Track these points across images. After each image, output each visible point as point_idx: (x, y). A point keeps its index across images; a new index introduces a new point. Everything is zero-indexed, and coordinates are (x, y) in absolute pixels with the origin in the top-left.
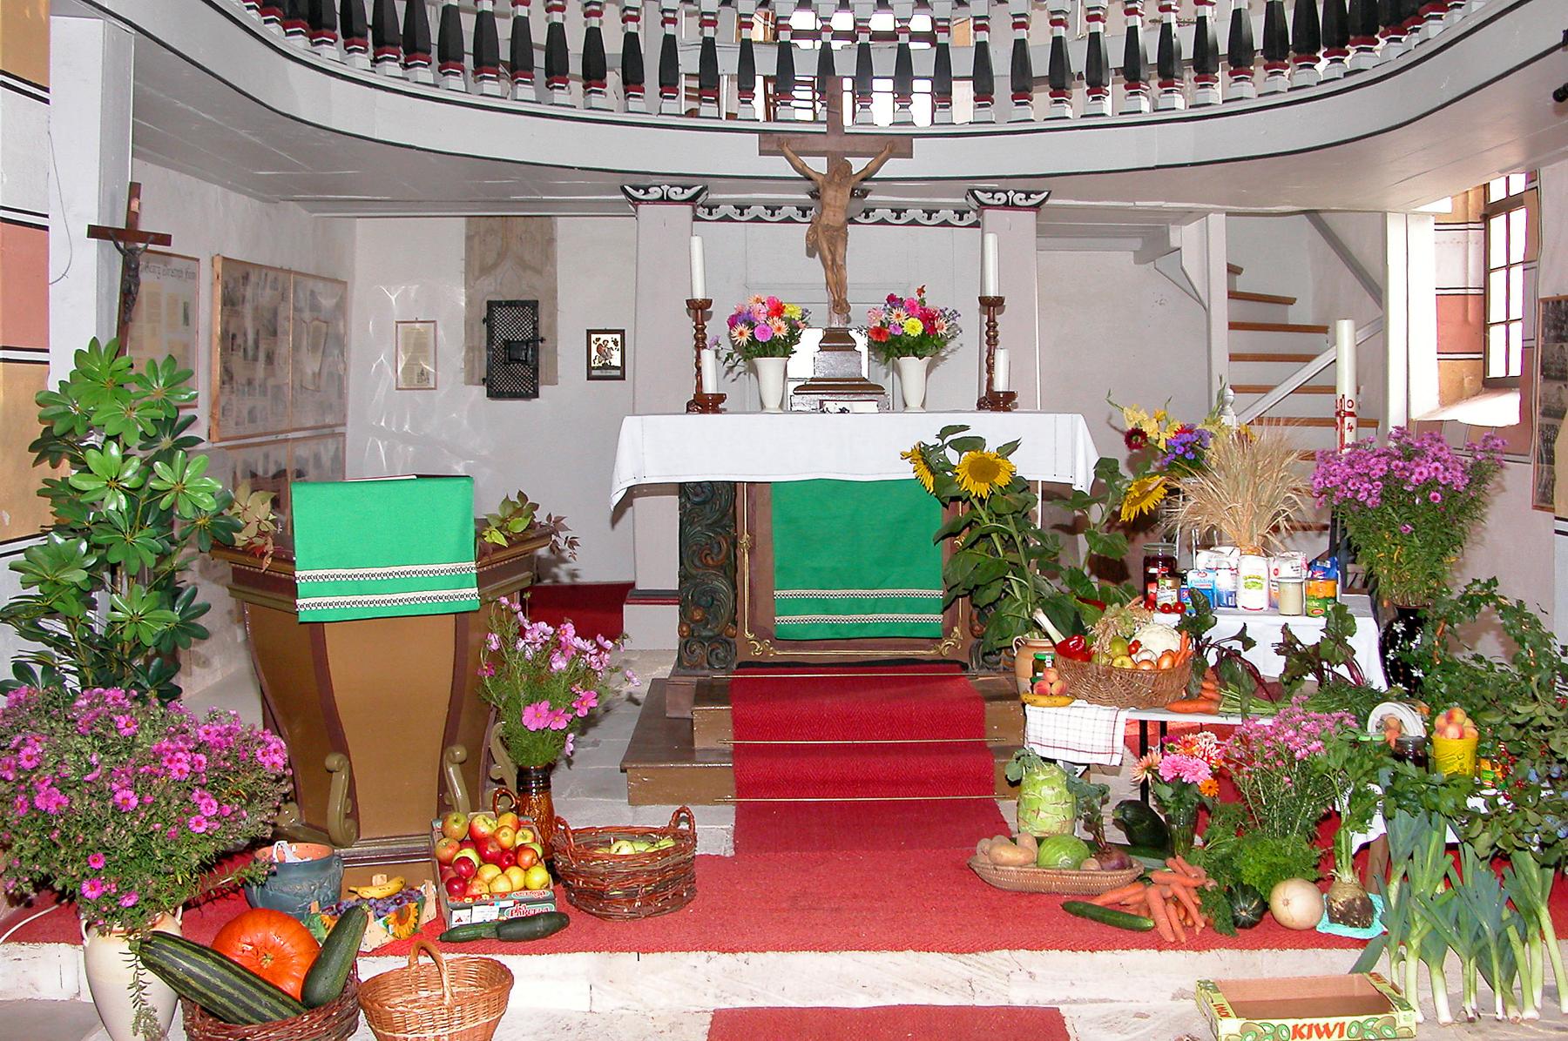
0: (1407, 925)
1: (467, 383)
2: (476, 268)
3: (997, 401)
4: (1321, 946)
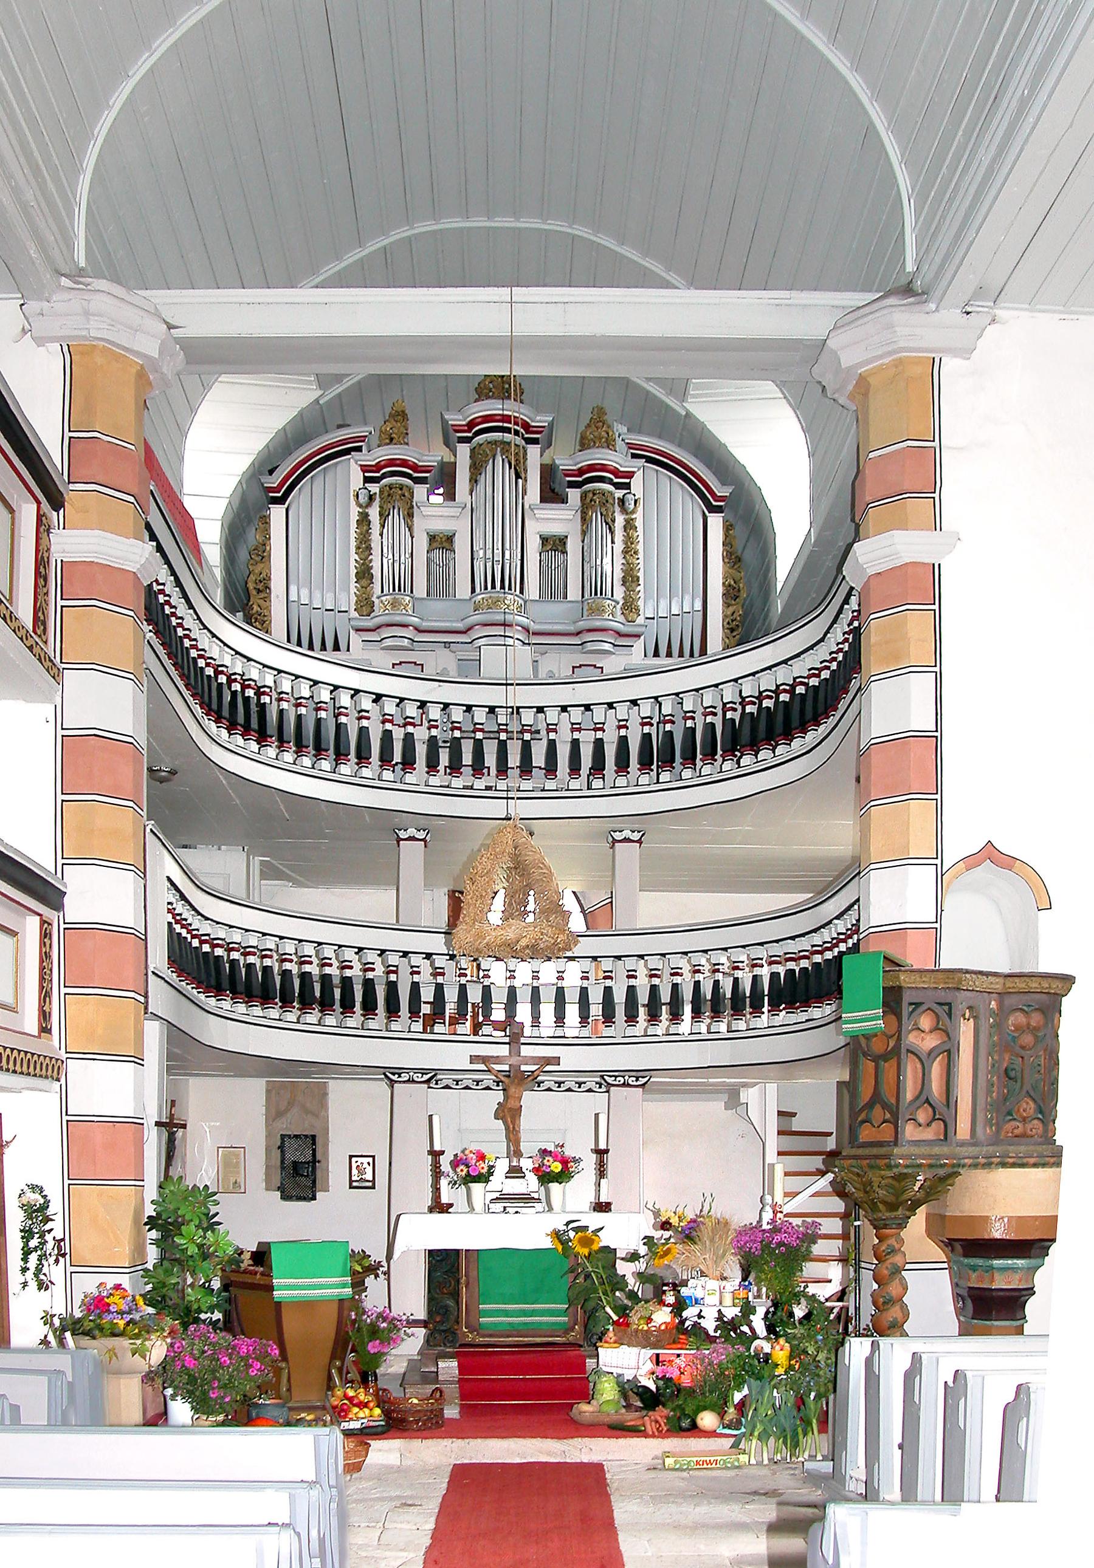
0: (754, 1427)
1: (267, 1189)
2: (274, 1113)
3: (602, 1207)
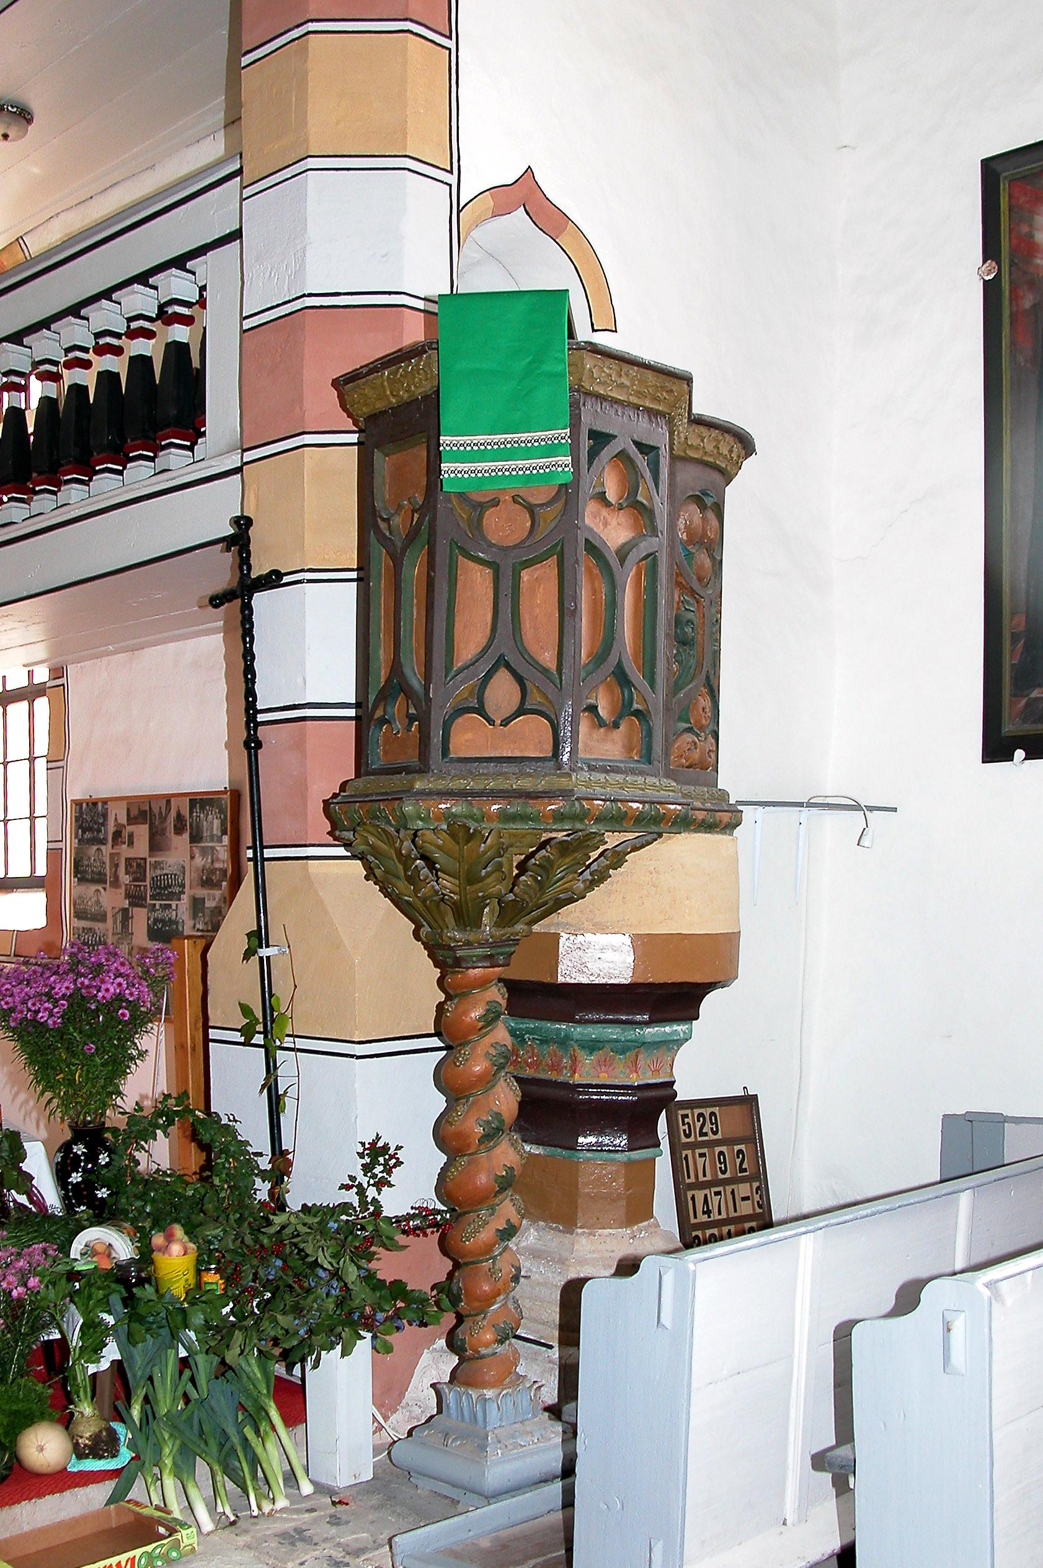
4: (77, 1485)
